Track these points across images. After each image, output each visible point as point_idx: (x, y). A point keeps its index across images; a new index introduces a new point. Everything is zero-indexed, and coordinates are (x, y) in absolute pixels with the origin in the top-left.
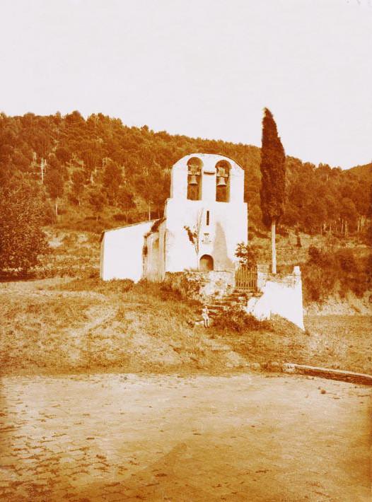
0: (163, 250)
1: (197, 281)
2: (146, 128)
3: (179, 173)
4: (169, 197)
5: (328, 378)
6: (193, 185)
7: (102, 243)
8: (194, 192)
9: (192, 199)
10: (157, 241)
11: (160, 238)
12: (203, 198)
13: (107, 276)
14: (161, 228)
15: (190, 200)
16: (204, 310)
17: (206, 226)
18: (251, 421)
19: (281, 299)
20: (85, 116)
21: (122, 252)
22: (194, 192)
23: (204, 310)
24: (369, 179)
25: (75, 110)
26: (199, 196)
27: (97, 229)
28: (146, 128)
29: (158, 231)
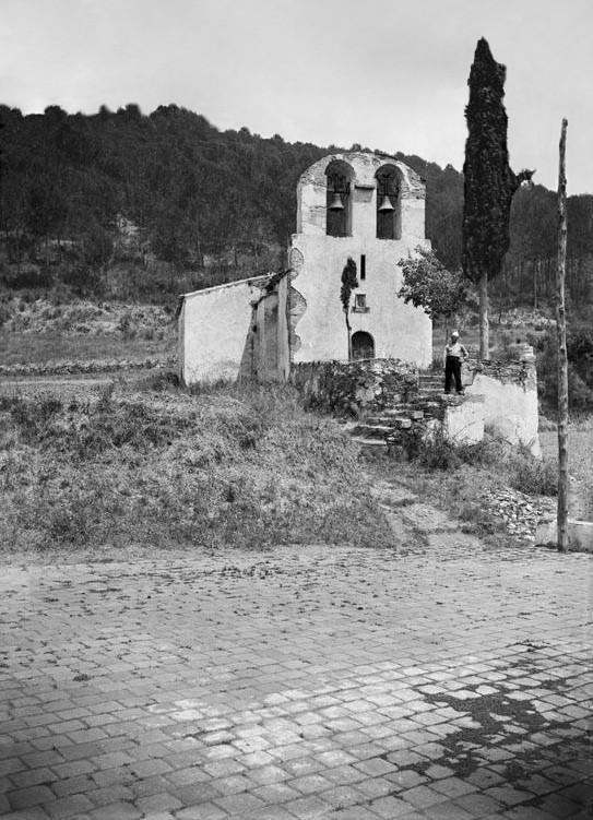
0: (286, 327)
1: (350, 376)
2: (103, 109)
3: (312, 196)
4: (295, 231)
5: (472, 113)
6: (337, 209)
7: (180, 317)
8: (338, 224)
9: (335, 235)
10: (275, 310)
11: (280, 304)
12: (353, 233)
13: (188, 378)
14: (282, 288)
17: (356, 291)
19: (501, 409)
20: (147, 109)
22: (338, 224)
25: (132, 101)
26: (348, 229)
27: (171, 300)
28: (103, 109)
29: (276, 293)
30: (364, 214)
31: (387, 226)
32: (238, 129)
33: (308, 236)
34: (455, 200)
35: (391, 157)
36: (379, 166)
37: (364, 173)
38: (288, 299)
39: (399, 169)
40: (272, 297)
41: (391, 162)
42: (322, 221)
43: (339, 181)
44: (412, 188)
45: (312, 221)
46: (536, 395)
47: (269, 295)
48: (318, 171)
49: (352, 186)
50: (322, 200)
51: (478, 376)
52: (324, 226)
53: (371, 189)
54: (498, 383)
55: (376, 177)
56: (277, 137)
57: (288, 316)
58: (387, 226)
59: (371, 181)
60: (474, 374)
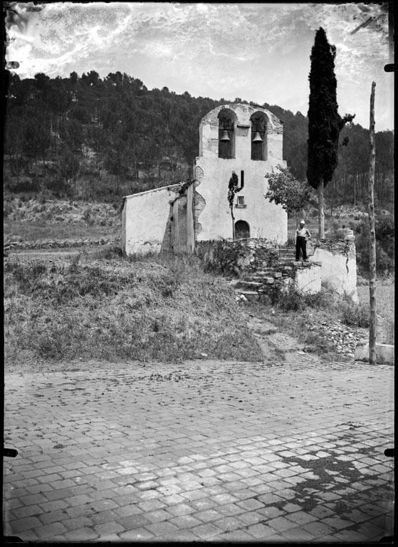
1: (234, 249)
3: (209, 132)
8: (226, 150)
9: (224, 158)
10: (185, 207)
12: (236, 156)
13: (128, 251)
14: (189, 192)
15: (221, 159)
16: (222, 332)
17: (237, 194)
18: (344, 434)
19: (333, 271)
20: (103, 76)
21: (145, 218)
22: (226, 150)
23: (222, 332)
24: (46, 537)
27: (117, 200)
28: (165, 88)
29: (186, 196)
30: (243, 144)
31: (258, 152)
32: (161, 89)
33: (207, 158)
34: (303, 135)
35: (261, 107)
36: (253, 112)
37: (243, 117)
38: (194, 199)
39: (266, 115)
40: (183, 198)
41: (261, 110)
42: (216, 148)
43: (226, 122)
44: (274, 127)
45: (209, 148)
46: (355, 262)
47: (181, 196)
48: (213, 116)
49: (235, 126)
50: (216, 135)
51: (317, 249)
52: (217, 151)
53: (248, 128)
54: (330, 254)
55: (251, 119)
56: (186, 93)
57: (194, 211)
58: (258, 152)
59: (248, 123)
60: (315, 248)
